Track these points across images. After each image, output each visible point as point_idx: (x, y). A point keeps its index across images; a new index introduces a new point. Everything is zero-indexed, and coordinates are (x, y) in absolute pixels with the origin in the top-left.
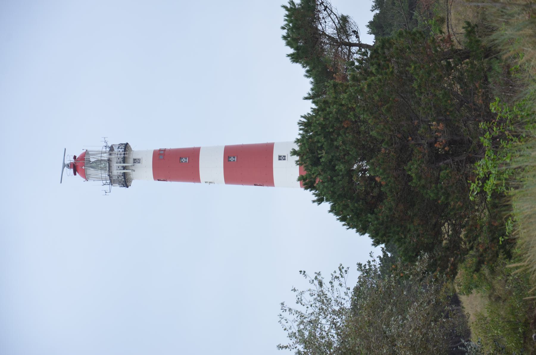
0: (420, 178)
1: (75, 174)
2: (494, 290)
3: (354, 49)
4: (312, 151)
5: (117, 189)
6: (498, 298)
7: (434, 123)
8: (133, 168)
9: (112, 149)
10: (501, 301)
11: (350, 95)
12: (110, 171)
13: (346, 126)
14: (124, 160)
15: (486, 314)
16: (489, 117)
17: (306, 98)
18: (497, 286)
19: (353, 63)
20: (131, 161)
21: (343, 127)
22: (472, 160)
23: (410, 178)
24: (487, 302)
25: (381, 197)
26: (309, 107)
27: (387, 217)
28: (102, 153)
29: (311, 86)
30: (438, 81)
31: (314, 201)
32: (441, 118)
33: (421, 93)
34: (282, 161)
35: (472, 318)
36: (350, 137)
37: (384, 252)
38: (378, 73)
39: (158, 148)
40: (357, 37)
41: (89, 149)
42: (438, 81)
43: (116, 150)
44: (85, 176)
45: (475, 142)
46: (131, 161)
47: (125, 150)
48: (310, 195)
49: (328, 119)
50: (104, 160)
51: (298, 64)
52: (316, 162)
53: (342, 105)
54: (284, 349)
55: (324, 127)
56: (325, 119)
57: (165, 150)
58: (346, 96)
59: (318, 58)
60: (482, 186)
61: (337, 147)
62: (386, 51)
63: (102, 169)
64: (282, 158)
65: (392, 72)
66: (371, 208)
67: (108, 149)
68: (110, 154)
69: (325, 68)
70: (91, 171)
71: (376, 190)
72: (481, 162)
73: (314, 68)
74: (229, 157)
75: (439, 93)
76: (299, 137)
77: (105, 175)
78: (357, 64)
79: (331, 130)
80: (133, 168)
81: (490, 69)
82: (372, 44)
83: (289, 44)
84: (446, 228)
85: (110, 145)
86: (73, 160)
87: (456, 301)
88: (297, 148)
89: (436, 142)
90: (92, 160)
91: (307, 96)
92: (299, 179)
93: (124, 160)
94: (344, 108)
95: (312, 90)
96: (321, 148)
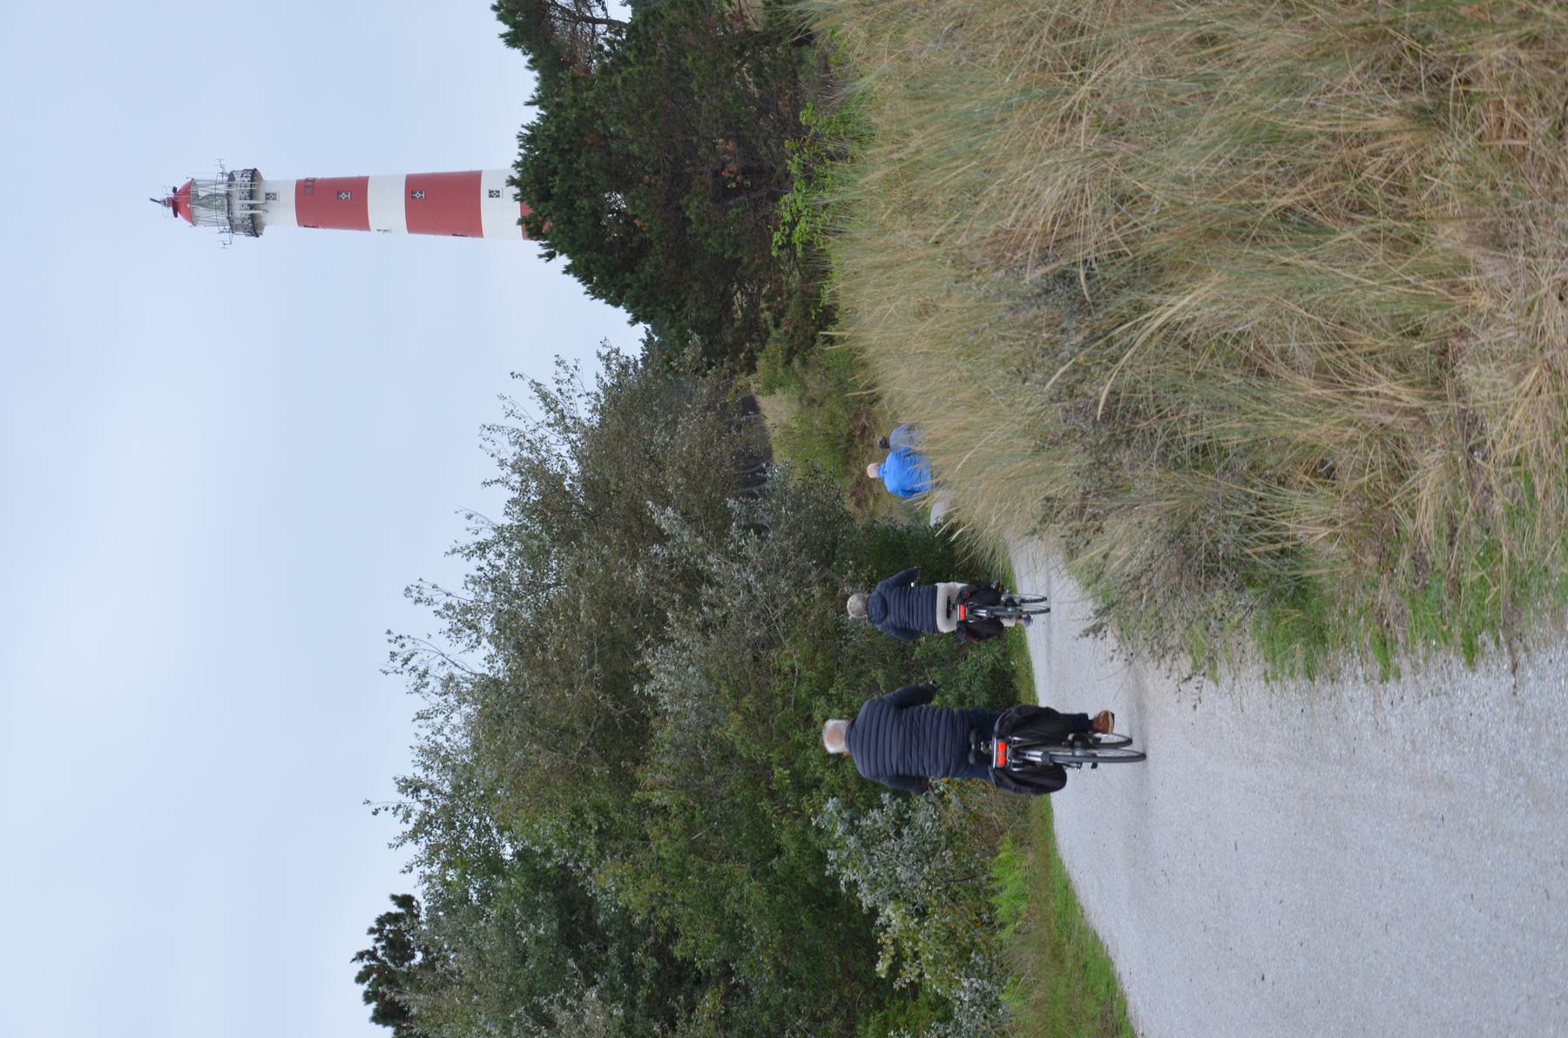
0: (702, 222)
1: (176, 216)
2: (806, 389)
3: (601, 28)
4: (539, 180)
5: (241, 239)
6: (812, 401)
7: (721, 140)
8: (265, 207)
9: (231, 177)
10: (816, 406)
11: (598, 94)
12: (229, 211)
13: (589, 142)
14: (252, 195)
15: (794, 425)
16: (799, 131)
17: (529, 104)
18: (811, 384)
19: (601, 47)
20: (262, 196)
21: (586, 143)
22: (775, 197)
23: (687, 221)
24: (796, 407)
25: (643, 249)
26: (533, 115)
27: (652, 276)
28: (217, 183)
29: (536, 84)
30: (727, 76)
31: (541, 256)
32: (731, 133)
33: (704, 97)
34: (495, 199)
35: (775, 434)
36: (597, 158)
37: (649, 335)
38: (638, 62)
39: (303, 177)
40: (604, 9)
41: (196, 177)
42: (727, 76)
43: (238, 179)
44: (191, 218)
45: (779, 170)
46: (262, 196)
47: (252, 180)
48: (535, 247)
49: (562, 129)
50: (220, 195)
51: (518, 59)
52: (546, 196)
53: (584, 109)
54: (493, 485)
55: (556, 142)
56: (559, 129)
57: (314, 180)
58: (591, 94)
59: (547, 41)
60: (790, 235)
61: (578, 173)
62: (649, 28)
63: (217, 208)
64: (492, 194)
65: (659, 62)
66: (629, 265)
67: (226, 178)
68: (230, 186)
69: (557, 56)
70: (200, 212)
71: (636, 239)
72: (787, 198)
73: (540, 56)
74: (413, 193)
75: (729, 96)
76: (519, 159)
77: (223, 217)
78: (607, 48)
79: (567, 147)
80: (265, 207)
81: (801, 61)
82: (627, 21)
83: (501, 18)
84: (739, 299)
85: (229, 172)
86: (172, 195)
87: (750, 405)
88: (517, 176)
89: (723, 169)
90: (202, 194)
91: (530, 99)
92: (520, 222)
93: (252, 195)
94: (588, 114)
95: (538, 90)
96: (554, 173)
